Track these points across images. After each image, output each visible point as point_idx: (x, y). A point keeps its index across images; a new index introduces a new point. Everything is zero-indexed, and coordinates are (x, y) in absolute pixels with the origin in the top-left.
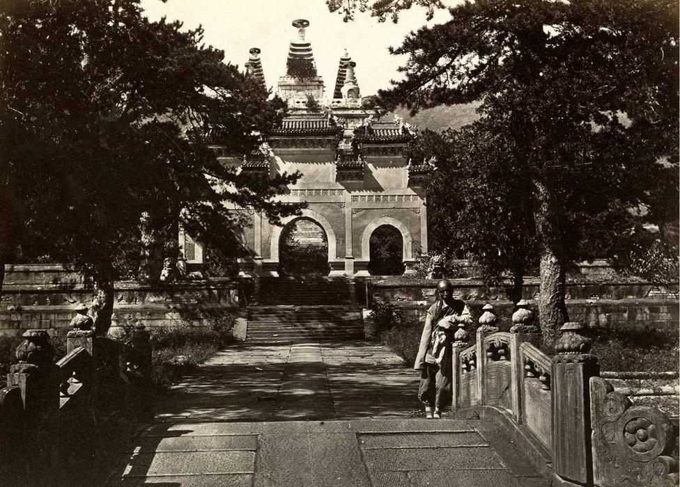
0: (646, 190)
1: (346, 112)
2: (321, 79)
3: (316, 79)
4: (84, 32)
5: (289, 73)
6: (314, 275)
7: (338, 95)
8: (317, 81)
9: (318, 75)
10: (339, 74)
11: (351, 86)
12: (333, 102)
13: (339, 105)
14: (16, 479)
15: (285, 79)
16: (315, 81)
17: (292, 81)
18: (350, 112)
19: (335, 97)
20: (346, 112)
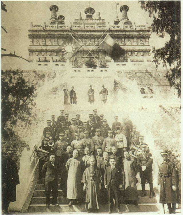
12: (114, 27)
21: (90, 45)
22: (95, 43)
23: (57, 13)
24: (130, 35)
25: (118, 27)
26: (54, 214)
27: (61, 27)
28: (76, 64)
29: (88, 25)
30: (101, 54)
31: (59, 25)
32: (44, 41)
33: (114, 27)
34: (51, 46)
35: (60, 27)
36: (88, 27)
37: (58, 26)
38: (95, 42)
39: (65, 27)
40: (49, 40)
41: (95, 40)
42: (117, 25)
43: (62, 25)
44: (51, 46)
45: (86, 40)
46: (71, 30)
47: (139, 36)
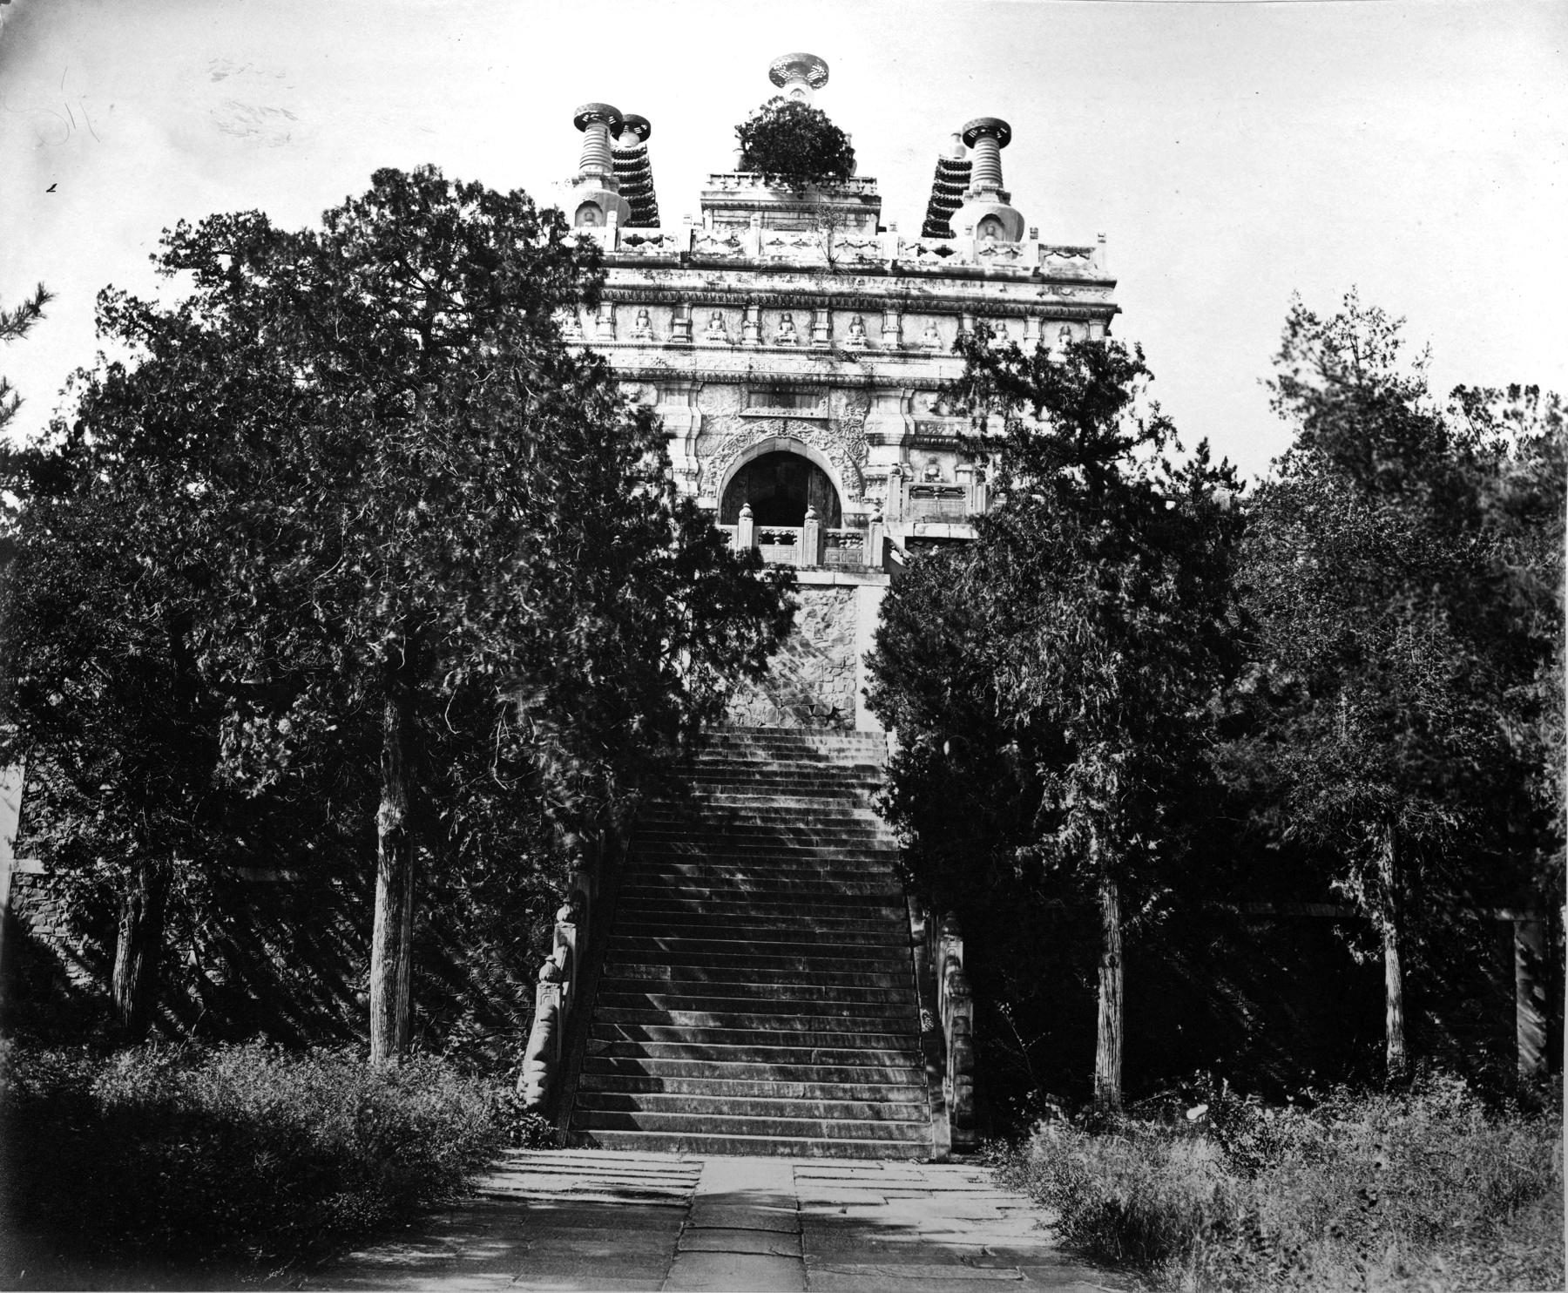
0: (1063, 738)
1: (973, 290)
2: (867, 190)
3: (853, 187)
4: (436, 319)
5: (748, 162)
6: (1093, 830)
7: (937, 224)
8: (856, 195)
9: (859, 172)
10: (931, 211)
11: (991, 204)
12: (922, 251)
13: (945, 262)
14: (1485, 540)
15: (731, 183)
16: (846, 196)
17: (760, 192)
18: (991, 291)
19: (925, 234)
20: (973, 290)
21: (786, 346)
22: (811, 335)
23: (1002, 151)
24: (1003, 301)
25: (944, 252)
26: (320, 1287)
27: (635, 241)
28: (1285, 469)
29: (782, 235)
30: (844, 401)
31: (628, 232)
32: (1034, 323)
33: (922, 251)
34: (790, 352)
35: (629, 241)
36: (641, 241)
37: (617, 234)
38: (813, 330)
39: (657, 241)
40: (783, 320)
41: (813, 322)
42: (938, 243)
43: (642, 232)
44: (790, 352)
45: (835, 319)
46: (689, 261)
47: (1055, 308)
